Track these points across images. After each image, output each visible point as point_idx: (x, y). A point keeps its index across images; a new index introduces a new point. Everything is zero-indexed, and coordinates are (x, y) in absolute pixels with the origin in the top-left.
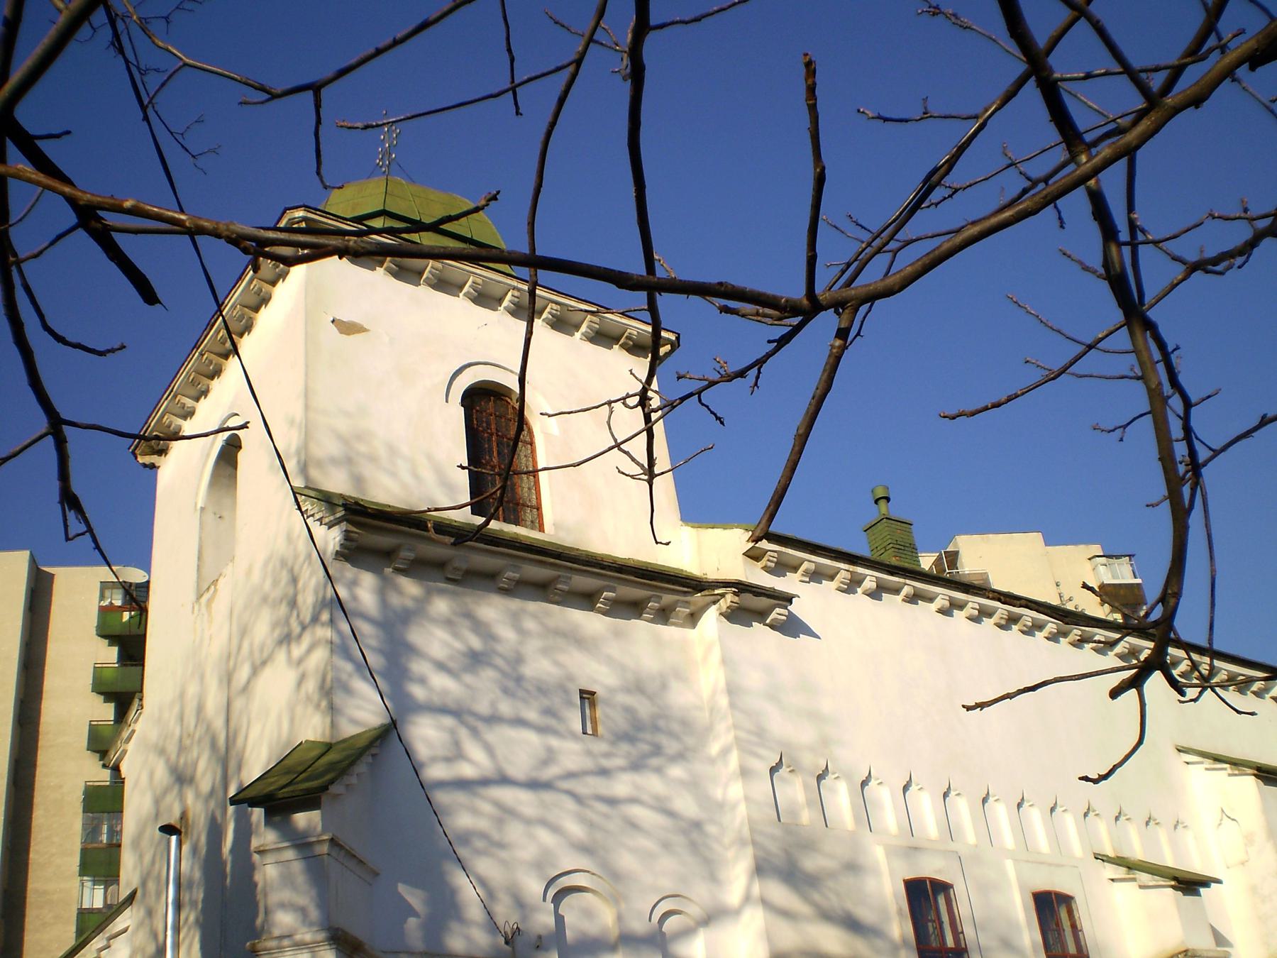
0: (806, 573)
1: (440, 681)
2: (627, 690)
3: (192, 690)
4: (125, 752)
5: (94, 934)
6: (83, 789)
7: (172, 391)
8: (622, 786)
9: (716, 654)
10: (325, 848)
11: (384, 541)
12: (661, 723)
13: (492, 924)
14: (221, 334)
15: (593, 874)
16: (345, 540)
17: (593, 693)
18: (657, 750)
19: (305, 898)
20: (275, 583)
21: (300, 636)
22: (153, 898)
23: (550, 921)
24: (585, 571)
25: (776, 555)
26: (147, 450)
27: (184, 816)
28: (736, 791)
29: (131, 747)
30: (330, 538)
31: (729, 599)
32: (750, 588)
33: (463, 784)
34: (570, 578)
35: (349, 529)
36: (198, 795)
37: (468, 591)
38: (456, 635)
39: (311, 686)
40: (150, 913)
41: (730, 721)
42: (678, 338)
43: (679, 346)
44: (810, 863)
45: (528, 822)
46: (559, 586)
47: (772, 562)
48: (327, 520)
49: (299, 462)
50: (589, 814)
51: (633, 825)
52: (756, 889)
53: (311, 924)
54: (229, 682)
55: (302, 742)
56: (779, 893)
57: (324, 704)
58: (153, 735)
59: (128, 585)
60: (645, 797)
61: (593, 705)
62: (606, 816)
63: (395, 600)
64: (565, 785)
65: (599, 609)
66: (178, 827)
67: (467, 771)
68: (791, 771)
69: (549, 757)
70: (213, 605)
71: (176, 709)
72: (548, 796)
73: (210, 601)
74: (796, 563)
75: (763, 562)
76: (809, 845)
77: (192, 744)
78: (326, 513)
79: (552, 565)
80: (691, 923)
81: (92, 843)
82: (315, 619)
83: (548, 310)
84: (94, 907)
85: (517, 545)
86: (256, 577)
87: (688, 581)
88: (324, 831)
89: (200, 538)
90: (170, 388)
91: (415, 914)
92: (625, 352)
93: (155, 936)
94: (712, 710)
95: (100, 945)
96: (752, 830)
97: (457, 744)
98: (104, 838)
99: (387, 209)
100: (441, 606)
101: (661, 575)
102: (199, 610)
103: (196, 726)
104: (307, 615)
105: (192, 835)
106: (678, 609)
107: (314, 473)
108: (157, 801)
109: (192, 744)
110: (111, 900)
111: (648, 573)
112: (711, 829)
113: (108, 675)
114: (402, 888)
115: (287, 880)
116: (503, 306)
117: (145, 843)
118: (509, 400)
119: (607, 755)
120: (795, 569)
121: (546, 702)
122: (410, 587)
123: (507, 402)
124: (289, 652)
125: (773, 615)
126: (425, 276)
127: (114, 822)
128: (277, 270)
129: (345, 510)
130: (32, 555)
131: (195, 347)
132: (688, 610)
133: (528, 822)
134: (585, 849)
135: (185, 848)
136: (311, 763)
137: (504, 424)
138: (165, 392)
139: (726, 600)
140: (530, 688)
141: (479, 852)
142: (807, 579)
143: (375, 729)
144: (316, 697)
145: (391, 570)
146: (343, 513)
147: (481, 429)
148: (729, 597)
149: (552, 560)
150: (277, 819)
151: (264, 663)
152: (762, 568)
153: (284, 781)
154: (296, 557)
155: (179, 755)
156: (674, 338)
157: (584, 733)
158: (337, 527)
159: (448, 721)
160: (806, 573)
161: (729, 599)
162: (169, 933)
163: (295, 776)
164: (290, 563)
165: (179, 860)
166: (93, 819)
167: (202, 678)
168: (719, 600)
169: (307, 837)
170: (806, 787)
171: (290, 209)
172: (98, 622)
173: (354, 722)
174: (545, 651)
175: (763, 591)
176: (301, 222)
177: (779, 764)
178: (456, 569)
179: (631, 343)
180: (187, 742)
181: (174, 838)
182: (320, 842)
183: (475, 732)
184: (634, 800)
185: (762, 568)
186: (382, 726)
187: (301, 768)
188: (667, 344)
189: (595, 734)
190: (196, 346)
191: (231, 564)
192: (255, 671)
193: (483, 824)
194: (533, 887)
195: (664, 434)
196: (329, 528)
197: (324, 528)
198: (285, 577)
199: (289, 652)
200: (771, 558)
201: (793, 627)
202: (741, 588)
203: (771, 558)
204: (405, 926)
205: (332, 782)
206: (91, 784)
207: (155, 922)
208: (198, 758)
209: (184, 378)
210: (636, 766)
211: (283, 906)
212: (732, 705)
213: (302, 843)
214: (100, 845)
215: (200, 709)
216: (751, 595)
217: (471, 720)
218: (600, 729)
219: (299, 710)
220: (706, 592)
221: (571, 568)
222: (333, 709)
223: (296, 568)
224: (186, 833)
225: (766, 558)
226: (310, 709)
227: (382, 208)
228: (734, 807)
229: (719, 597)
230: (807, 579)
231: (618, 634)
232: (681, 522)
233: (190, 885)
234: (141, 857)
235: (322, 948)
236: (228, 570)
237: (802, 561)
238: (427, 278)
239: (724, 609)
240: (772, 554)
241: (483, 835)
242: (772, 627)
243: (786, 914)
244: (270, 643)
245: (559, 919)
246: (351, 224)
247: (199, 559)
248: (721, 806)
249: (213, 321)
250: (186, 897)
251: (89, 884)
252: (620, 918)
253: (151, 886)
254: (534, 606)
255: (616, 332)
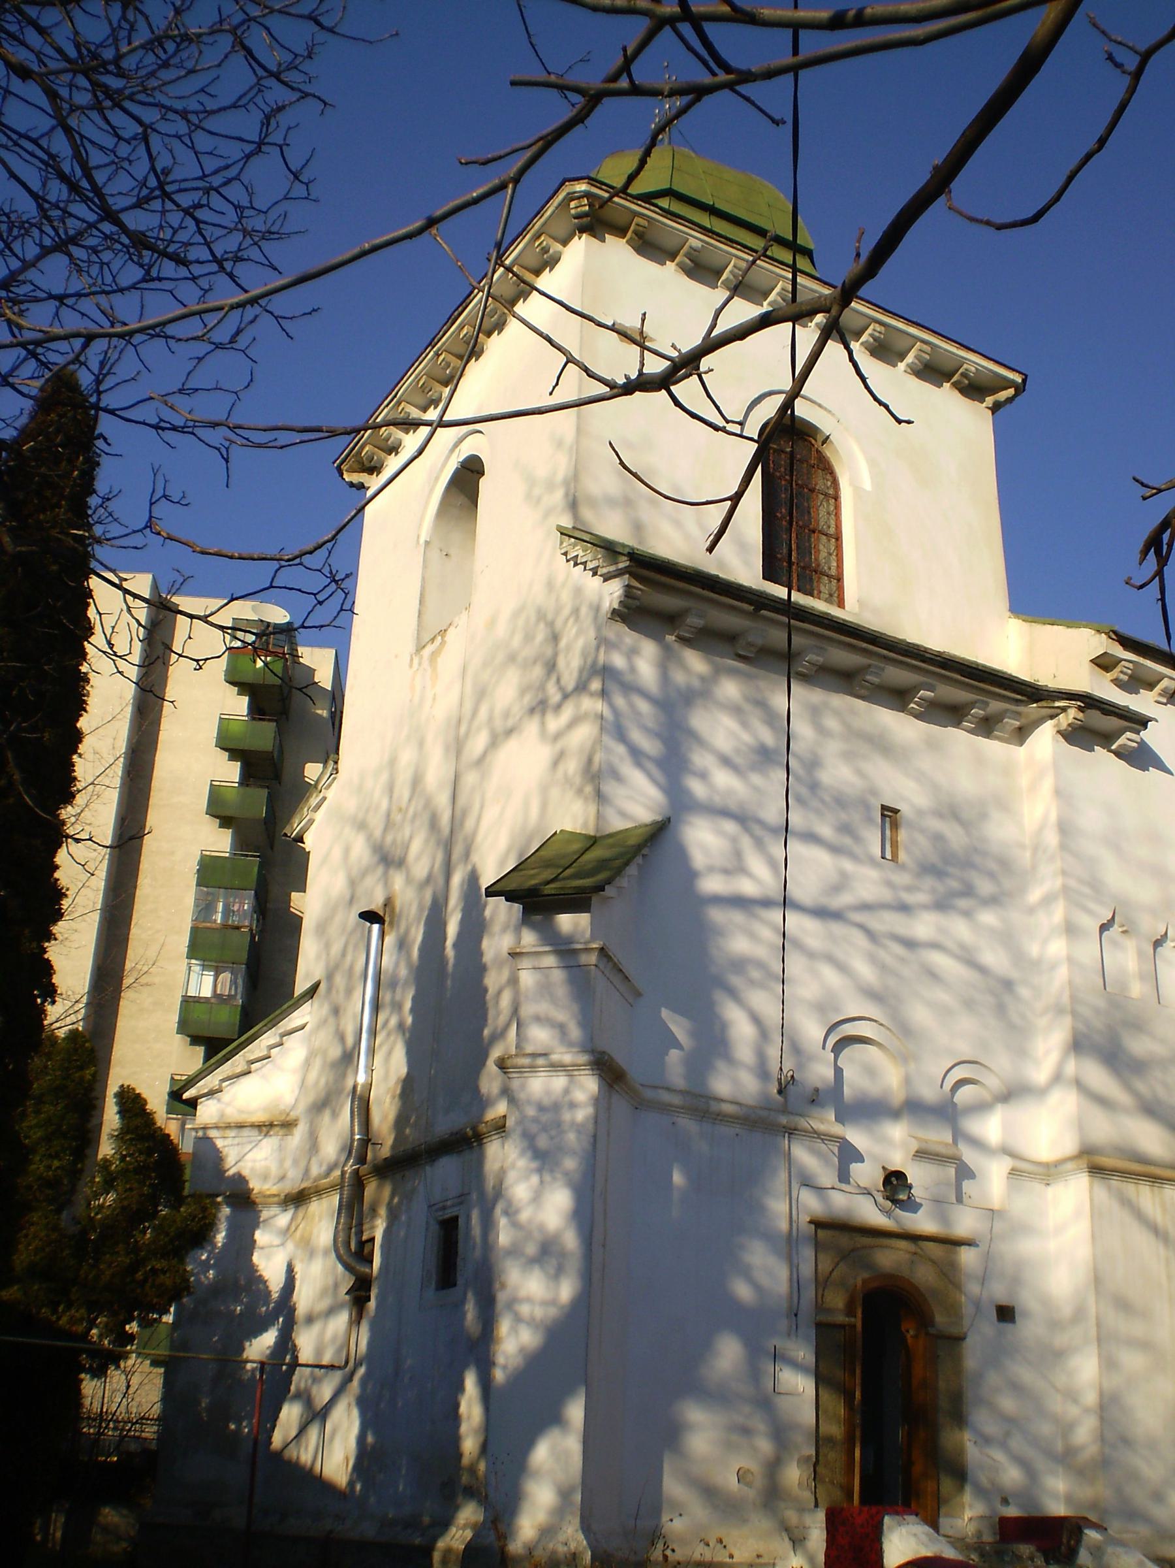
0: (1164, 692)
1: (723, 779)
2: (939, 814)
3: (407, 757)
4: (311, 822)
5: (265, 1028)
6: (199, 858)
7: (395, 396)
8: (923, 927)
9: (1048, 784)
10: (593, 958)
11: (668, 602)
12: (977, 859)
13: (762, 1072)
14: (465, 331)
15: (881, 1025)
16: (626, 596)
17: (896, 811)
18: (968, 891)
19: (565, 1014)
20: (528, 638)
21: (558, 707)
22: (342, 995)
23: (829, 1073)
24: (901, 662)
25: (1130, 665)
26: (356, 466)
27: (388, 903)
28: (1057, 947)
29: (319, 816)
30: (612, 593)
31: (1072, 715)
32: (1099, 704)
33: (739, 902)
34: (883, 669)
35: (632, 584)
36: (409, 880)
37: (762, 672)
38: (745, 724)
39: (572, 766)
40: (336, 1011)
41: (1058, 864)
42: (1024, 381)
43: (1024, 390)
44: (1138, 1046)
45: (811, 955)
46: (868, 677)
47: (1125, 674)
48: (604, 570)
49: (567, 495)
50: (882, 954)
51: (933, 975)
52: (1071, 1067)
53: (570, 1044)
54: (459, 753)
55: (556, 833)
56: (1098, 1076)
57: (589, 789)
58: (351, 805)
59: (265, 624)
60: (949, 944)
61: (895, 826)
62: (902, 960)
63: (679, 678)
64: (858, 917)
65: (913, 711)
66: (381, 914)
67: (747, 888)
68: (1124, 932)
69: (841, 884)
70: (439, 660)
71: (384, 777)
72: (837, 928)
73: (434, 655)
74: (1152, 679)
75: (1115, 674)
76: (1138, 1025)
77: (404, 820)
78: (604, 561)
79: (864, 650)
80: (987, 1096)
81: (204, 922)
82: (581, 687)
83: (869, 331)
84: (201, 995)
85: (826, 621)
86: (501, 630)
87: (1023, 687)
88: (593, 938)
89: (423, 578)
90: (394, 393)
91: (679, 1046)
92: (957, 392)
93: (342, 1038)
94: (1036, 849)
95: (272, 1041)
96: (1074, 998)
97: (738, 854)
98: (219, 918)
99: (675, 188)
100: (730, 689)
101: (991, 677)
102: (420, 664)
103: (410, 800)
104: (570, 681)
105: (398, 927)
106: (1006, 720)
107: (587, 514)
108: (353, 883)
109: (404, 820)
110: (221, 990)
111: (977, 672)
112: (1024, 992)
113: (235, 728)
114: (665, 1013)
115: (545, 989)
116: (814, 322)
117: (334, 929)
118: (813, 442)
119: (909, 889)
120: (1150, 686)
121: (843, 816)
122: (696, 662)
123: (811, 442)
124: (543, 724)
125: (1122, 740)
126: (723, 278)
127: (231, 900)
128: (545, 256)
129: (630, 560)
130: (154, 580)
131: (430, 344)
132: (1018, 723)
133: (811, 955)
134: (874, 995)
135: (388, 940)
136: (575, 857)
137: (805, 470)
138: (387, 398)
139: (1067, 716)
140: (827, 799)
141: (752, 983)
142: (1165, 701)
143: (646, 825)
144: (578, 780)
145: (674, 638)
146: (628, 563)
147: (778, 474)
148: (1072, 713)
149: (865, 645)
150: (538, 918)
151: (509, 732)
152: (1112, 681)
153: (548, 874)
154: (558, 611)
155: (386, 829)
156: (1020, 381)
157: (883, 858)
158: (617, 579)
159: (730, 827)
160: (1164, 692)
161: (1072, 715)
162: (364, 1036)
163: (561, 870)
164: (550, 617)
165: (380, 953)
166: (208, 894)
167: (421, 744)
168: (1057, 715)
169: (572, 943)
170: (1140, 954)
171: (570, 180)
172: (227, 665)
173: (623, 814)
174: (848, 756)
175: (1112, 708)
176: (582, 197)
177: (1111, 922)
178: (751, 645)
179: (966, 382)
180: (397, 817)
181: (376, 927)
182: (588, 950)
183: (759, 844)
184: (935, 946)
185: (1112, 681)
186: (654, 823)
187: (566, 862)
188: (1010, 388)
189: (895, 858)
190: (432, 344)
191: (465, 613)
192: (495, 742)
193: (760, 952)
194: (812, 1031)
195: (997, 501)
196: (605, 580)
197: (598, 580)
198: (541, 635)
199: (543, 724)
200: (1125, 670)
201: (1142, 758)
202: (1088, 702)
203: (1125, 670)
204: (667, 1058)
205: (609, 881)
206: (208, 853)
207: (343, 1022)
208: (411, 838)
209: (414, 380)
210: (941, 905)
211: (538, 1019)
212: (1063, 847)
213: (565, 950)
214: (214, 925)
215: (417, 782)
216: (1098, 713)
217: (758, 830)
218: (902, 856)
219: (555, 793)
220: (1043, 704)
221: (885, 657)
222: (600, 797)
223: (559, 623)
224: (391, 923)
225: (1118, 669)
226: (570, 794)
227: (668, 186)
228: (1053, 967)
229: (1059, 711)
230: (1165, 701)
231: (932, 745)
232: (1008, 614)
233: (393, 985)
234: (327, 946)
235: (582, 1073)
236: (462, 619)
237: (1162, 677)
238: (727, 279)
239: (1064, 726)
240: (1127, 664)
241: (760, 965)
242: (1118, 754)
243: (1102, 1101)
244: (517, 711)
245: (838, 1072)
246: (643, 204)
247: (421, 602)
248: (1036, 965)
249: (456, 313)
250: (386, 996)
251: (197, 969)
252: (907, 1081)
253: (340, 980)
254: (840, 701)
255: (948, 366)
